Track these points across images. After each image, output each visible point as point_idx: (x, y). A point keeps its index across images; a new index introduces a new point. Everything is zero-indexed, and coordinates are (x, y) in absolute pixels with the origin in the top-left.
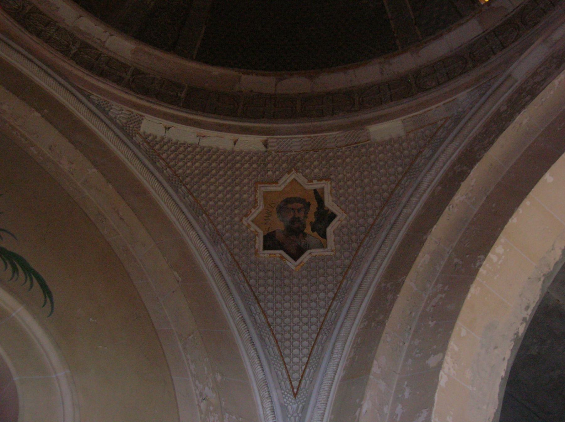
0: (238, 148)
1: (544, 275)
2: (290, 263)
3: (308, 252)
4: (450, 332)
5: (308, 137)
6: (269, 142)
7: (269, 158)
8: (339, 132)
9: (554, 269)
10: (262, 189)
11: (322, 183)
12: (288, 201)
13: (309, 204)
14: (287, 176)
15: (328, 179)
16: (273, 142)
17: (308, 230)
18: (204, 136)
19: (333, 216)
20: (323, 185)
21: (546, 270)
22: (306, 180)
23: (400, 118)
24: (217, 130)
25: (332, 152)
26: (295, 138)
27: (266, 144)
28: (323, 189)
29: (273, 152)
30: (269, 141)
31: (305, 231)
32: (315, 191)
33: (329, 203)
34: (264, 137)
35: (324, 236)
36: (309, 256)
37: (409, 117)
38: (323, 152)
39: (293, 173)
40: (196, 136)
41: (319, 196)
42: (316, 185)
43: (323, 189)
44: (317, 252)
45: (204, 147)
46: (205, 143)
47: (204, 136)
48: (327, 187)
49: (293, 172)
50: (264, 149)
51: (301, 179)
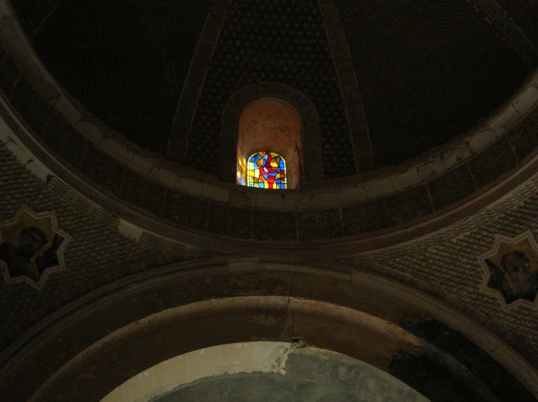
0: (30, 167)
1: (155, 396)
2: (6, 275)
3: (24, 277)
4: (254, 338)
5: (80, 195)
6: (53, 180)
7: (45, 191)
8: (101, 208)
9: (162, 395)
10: (24, 210)
11: (66, 235)
12: (34, 229)
13: (46, 242)
14: (46, 212)
15: (71, 234)
16: (54, 181)
17: (33, 260)
18: (12, 141)
19: (55, 262)
20: (65, 237)
21: (158, 393)
22: (57, 225)
23: (144, 230)
24: (25, 144)
25: (92, 259)
26: (71, 190)
27: (49, 178)
28: (63, 239)
29: (50, 189)
30: (53, 178)
31: (31, 259)
32: (57, 235)
33: (60, 252)
34: (52, 173)
35: (41, 272)
36: (22, 280)
37: (150, 234)
38: (81, 213)
39: (52, 214)
40: (8, 136)
41: (58, 241)
42: (61, 233)
43: (63, 239)
44: (29, 281)
45: (7, 150)
46: (10, 147)
47: (12, 141)
48: (68, 239)
49: (53, 213)
50: (44, 180)
51: (54, 222)
